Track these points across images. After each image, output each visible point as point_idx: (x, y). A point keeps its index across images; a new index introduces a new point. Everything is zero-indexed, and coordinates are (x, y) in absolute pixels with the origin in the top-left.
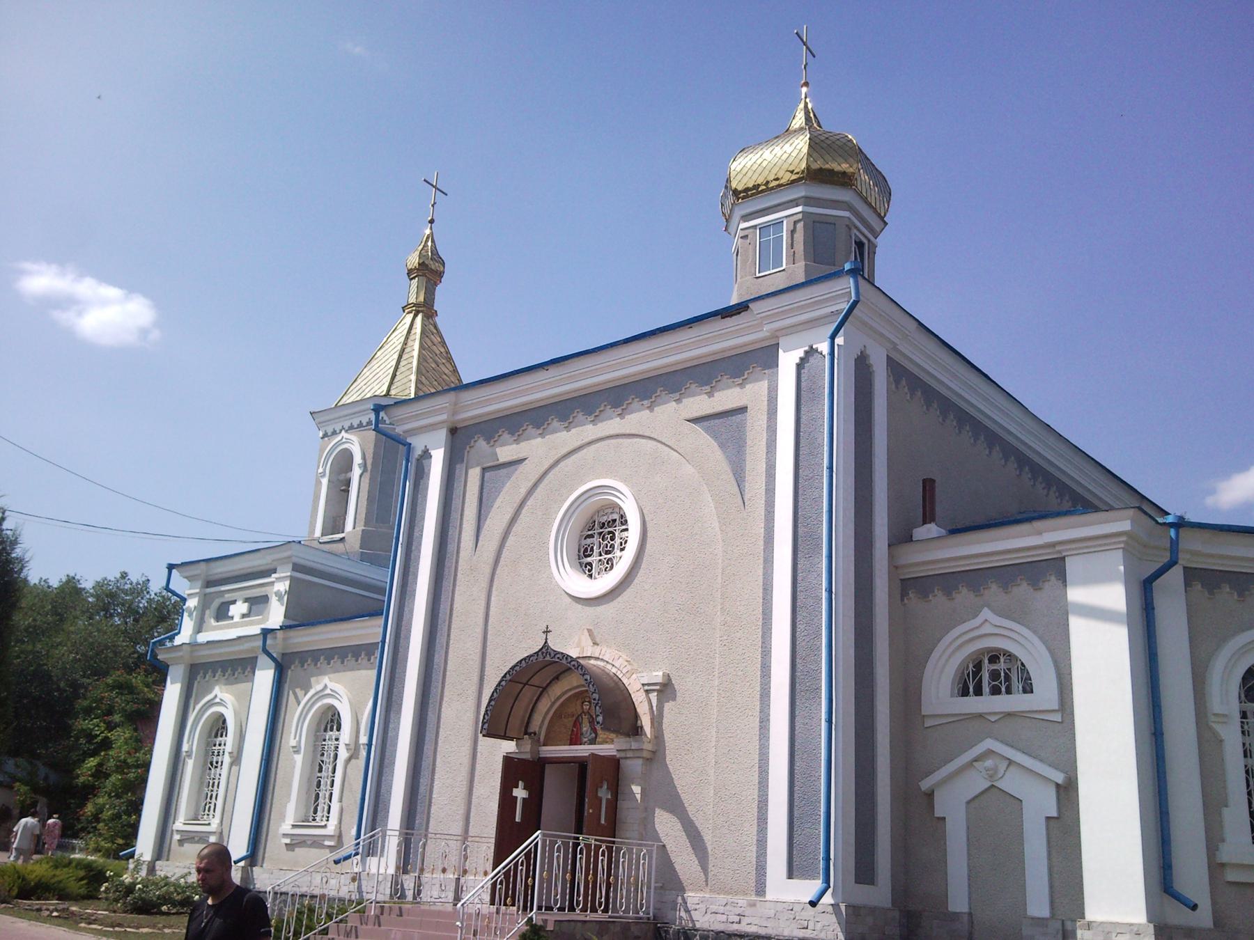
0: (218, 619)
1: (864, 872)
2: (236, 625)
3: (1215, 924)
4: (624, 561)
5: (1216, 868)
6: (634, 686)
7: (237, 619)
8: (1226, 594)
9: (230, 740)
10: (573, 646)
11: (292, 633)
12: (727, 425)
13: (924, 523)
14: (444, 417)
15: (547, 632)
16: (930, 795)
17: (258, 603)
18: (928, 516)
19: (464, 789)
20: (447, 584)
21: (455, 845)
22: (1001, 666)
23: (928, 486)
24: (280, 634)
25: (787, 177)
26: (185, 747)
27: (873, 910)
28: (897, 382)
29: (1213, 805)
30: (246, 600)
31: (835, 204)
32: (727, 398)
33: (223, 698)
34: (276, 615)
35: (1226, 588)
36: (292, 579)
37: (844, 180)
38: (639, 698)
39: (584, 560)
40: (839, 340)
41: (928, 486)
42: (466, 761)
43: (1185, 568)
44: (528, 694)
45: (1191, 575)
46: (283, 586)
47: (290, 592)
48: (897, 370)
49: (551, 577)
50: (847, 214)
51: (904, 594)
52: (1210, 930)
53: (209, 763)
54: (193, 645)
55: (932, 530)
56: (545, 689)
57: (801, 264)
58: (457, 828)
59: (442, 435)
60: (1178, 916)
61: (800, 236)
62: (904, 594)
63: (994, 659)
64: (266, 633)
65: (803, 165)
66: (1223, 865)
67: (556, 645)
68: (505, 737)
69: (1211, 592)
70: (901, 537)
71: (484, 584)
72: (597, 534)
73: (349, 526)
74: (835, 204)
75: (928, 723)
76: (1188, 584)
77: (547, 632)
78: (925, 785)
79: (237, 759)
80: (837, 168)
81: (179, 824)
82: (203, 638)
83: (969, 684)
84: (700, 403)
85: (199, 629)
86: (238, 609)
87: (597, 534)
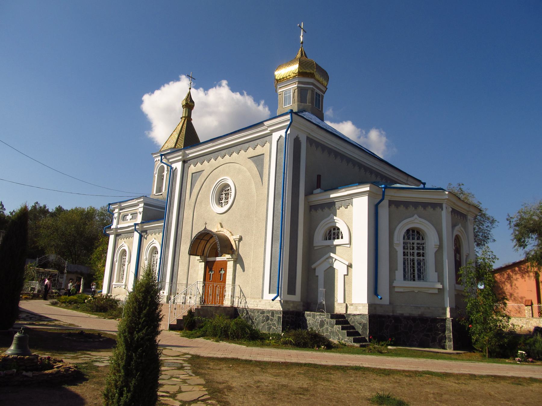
0: (123, 220)
1: (291, 290)
2: (128, 222)
3: (390, 303)
4: (230, 201)
5: (392, 287)
6: (231, 239)
7: (129, 220)
8: (402, 208)
9: (127, 258)
10: (215, 229)
11: (143, 225)
12: (258, 160)
13: (317, 188)
14: (181, 157)
15: (206, 224)
16: (315, 269)
17: (134, 215)
18: (319, 186)
19: (187, 271)
20: (181, 210)
21: (184, 287)
22: (336, 231)
23: (319, 177)
24: (140, 225)
25: (293, 75)
26: (115, 260)
27: (293, 302)
28: (311, 145)
29: (392, 270)
30: (131, 214)
31: (308, 83)
32: (259, 150)
33: (123, 244)
34: (139, 219)
35: (402, 206)
36: (144, 208)
37: (311, 75)
38: (233, 243)
39: (219, 201)
40: (289, 132)
41: (319, 177)
42: (187, 262)
43: (389, 201)
44: (203, 242)
45: (391, 203)
46: (141, 210)
47: (143, 212)
48: (310, 141)
49: (210, 207)
50: (312, 86)
51: (310, 210)
52: (388, 305)
53: (122, 265)
54: (117, 229)
55: (319, 190)
56: (208, 241)
57: (296, 103)
58: (185, 282)
59: (180, 163)
60: (377, 301)
61: (296, 94)
62: (310, 210)
63: (334, 229)
64: (136, 225)
65: (297, 71)
66: (394, 287)
67: (209, 228)
68: (196, 255)
69: (397, 208)
70: (309, 193)
71: (192, 210)
72: (223, 193)
73: (163, 190)
74: (308, 83)
75: (315, 248)
76: (390, 205)
77: (206, 224)
78: (313, 266)
79: (130, 262)
80: (308, 71)
81: (114, 283)
82: (119, 226)
83: (487, 227)
84: (251, 152)
85: (118, 224)
86: (129, 217)
87: (223, 193)
